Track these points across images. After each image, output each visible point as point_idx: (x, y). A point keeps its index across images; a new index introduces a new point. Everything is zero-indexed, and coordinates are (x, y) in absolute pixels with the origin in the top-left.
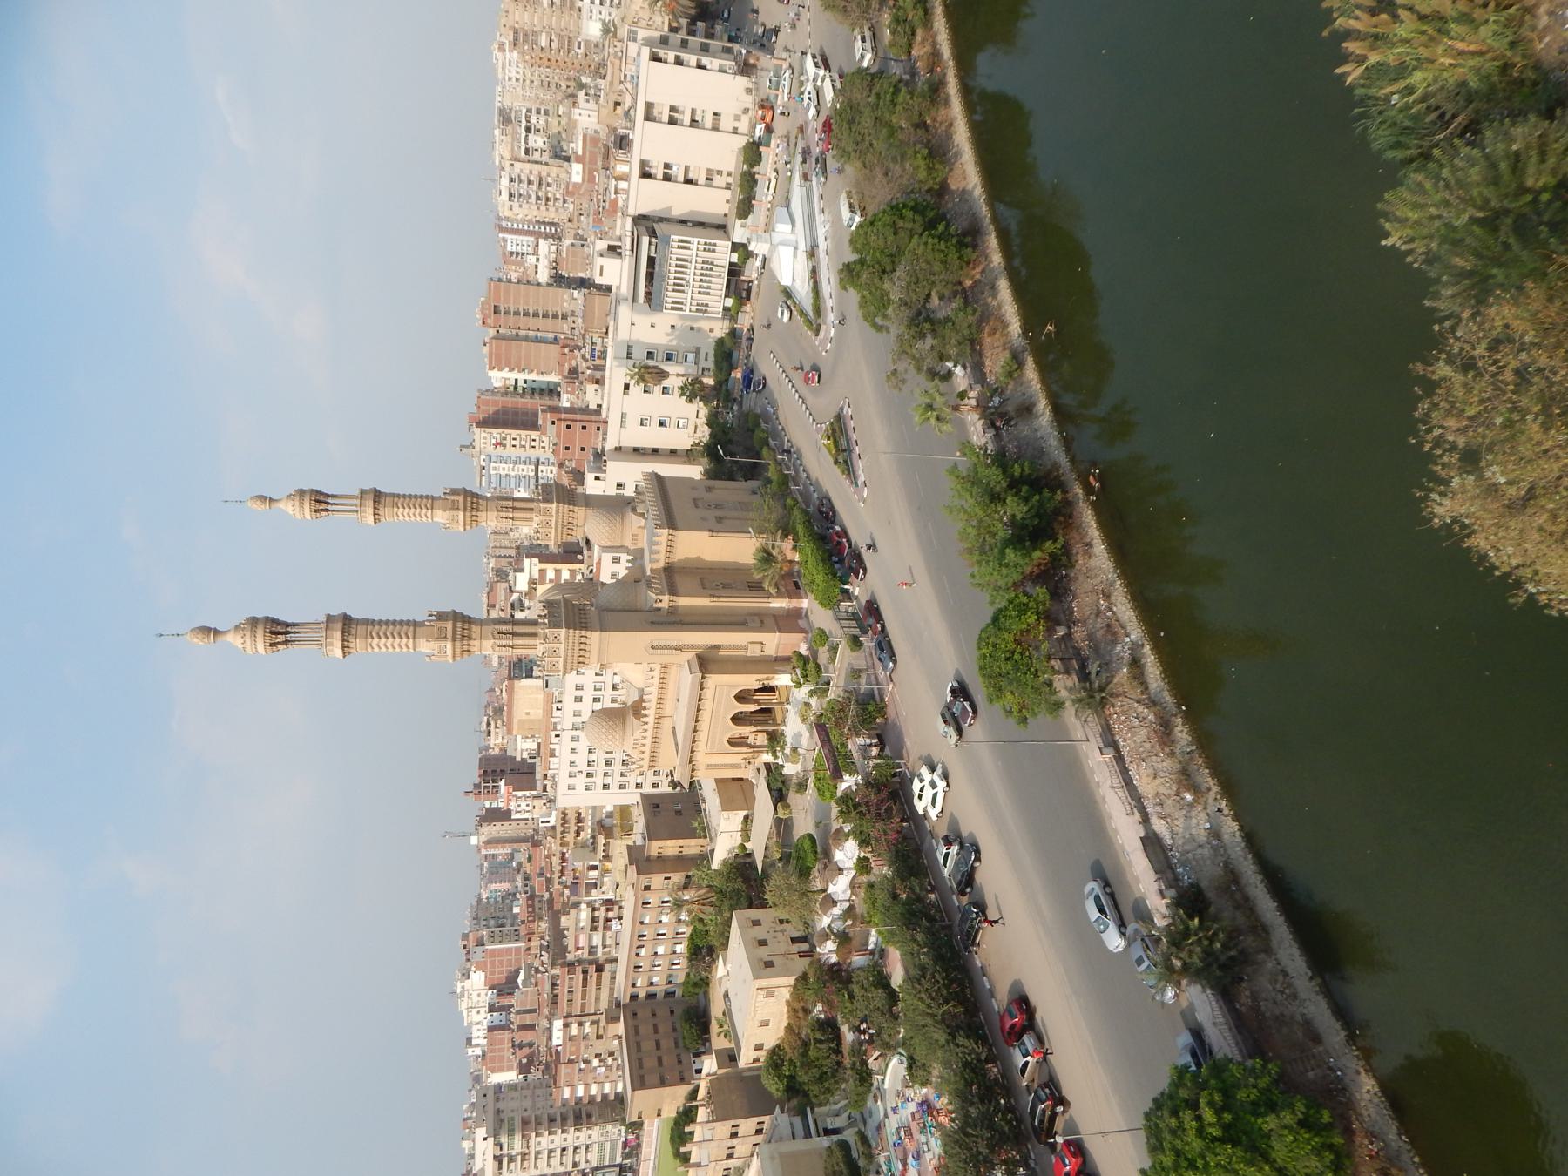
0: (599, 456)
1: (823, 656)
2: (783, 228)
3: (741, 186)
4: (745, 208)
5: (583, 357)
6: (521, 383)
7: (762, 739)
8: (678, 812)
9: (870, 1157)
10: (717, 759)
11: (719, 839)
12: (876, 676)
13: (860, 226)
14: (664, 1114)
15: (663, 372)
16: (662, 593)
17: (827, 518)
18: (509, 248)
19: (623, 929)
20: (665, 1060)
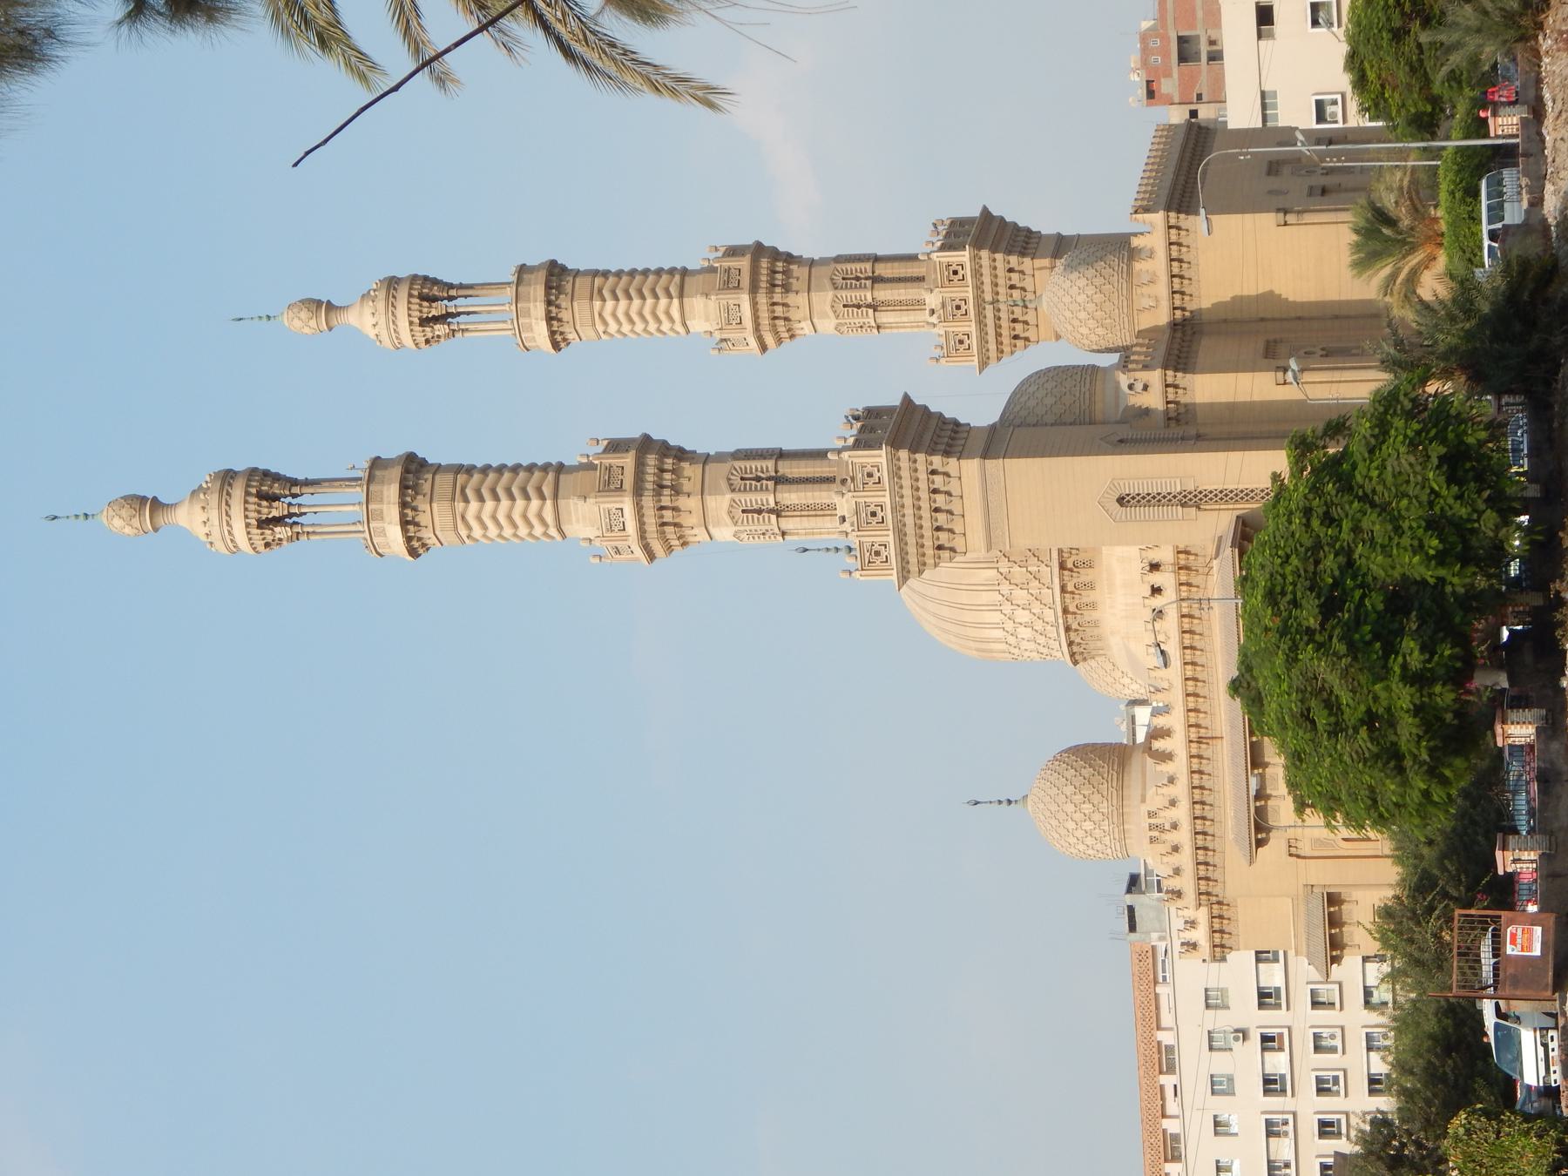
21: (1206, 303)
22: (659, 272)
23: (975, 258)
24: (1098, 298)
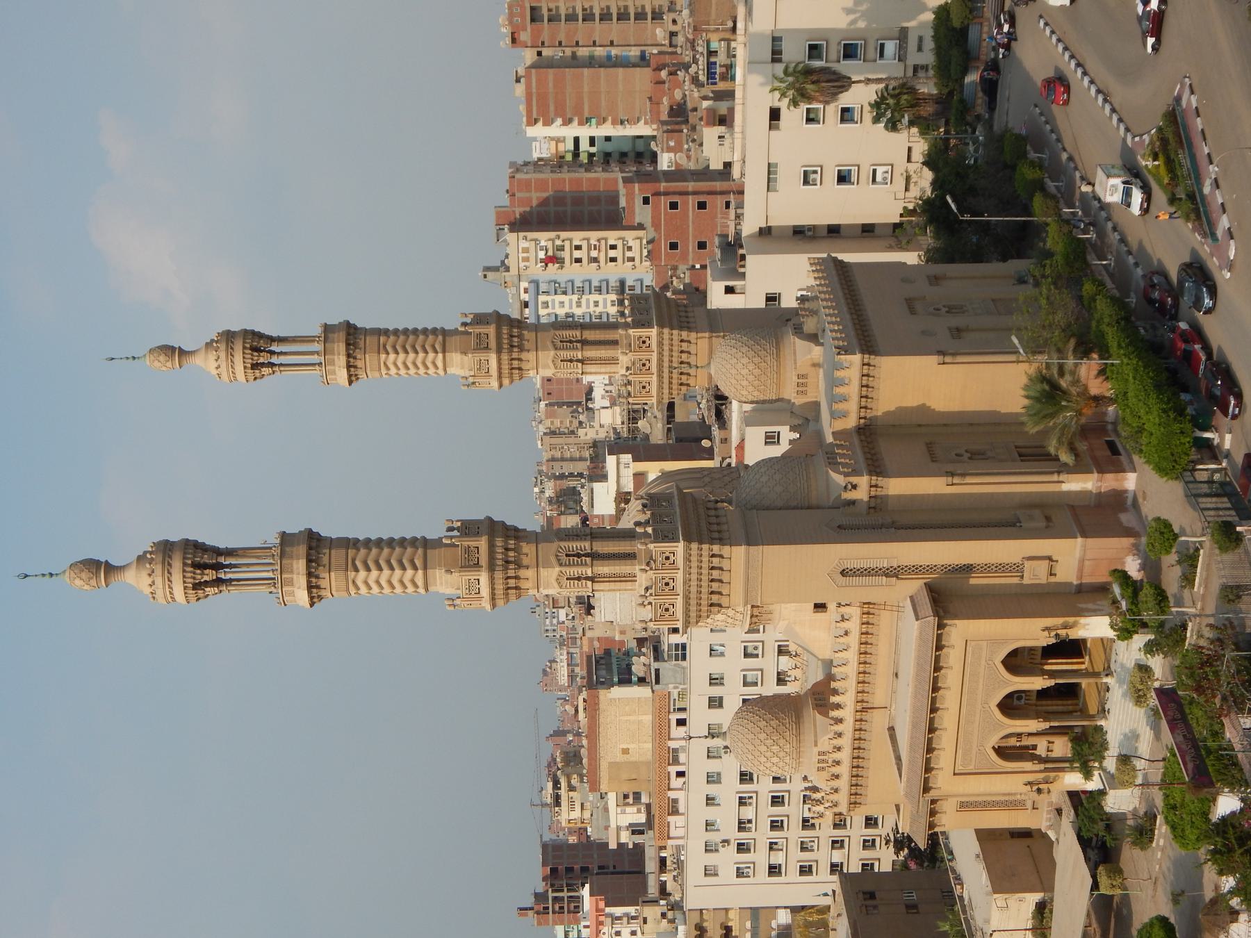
0: (733, 251)
1: (1171, 577)
5: (695, 80)
6: (584, 146)
7: (1061, 746)
8: (911, 907)
10: (980, 792)
16: (856, 472)
21: (880, 414)
22: (425, 331)
23: (660, 334)
24: (757, 372)
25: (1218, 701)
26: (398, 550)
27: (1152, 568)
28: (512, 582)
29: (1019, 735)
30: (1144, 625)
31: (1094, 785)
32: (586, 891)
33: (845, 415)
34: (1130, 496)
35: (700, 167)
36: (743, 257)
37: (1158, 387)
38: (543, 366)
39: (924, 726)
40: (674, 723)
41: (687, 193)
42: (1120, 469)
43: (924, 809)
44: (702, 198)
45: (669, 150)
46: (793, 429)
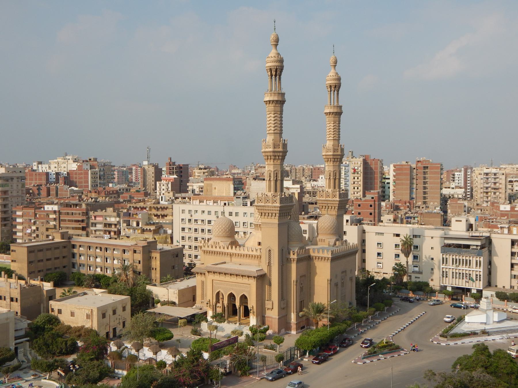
0: (359, 222)
1: (268, 342)
2: (496, 317)
3: (514, 294)
4: (502, 296)
5: (406, 213)
6: (387, 181)
7: (219, 310)
8: (173, 267)
9: (7, 372)
10: (208, 288)
11: (165, 289)
12: (263, 370)
13: (510, 355)
14: (13, 264)
15: (409, 254)
16: (298, 255)
17: (342, 343)
18: (456, 173)
19: (106, 240)
20: (41, 264)
23: (337, 201)
25: (234, 354)
26: (279, 126)
27: (270, 337)
28: (269, 157)
29: (223, 299)
30: (254, 335)
31: (209, 318)
32: (175, 176)
33: (314, 252)
34: (289, 332)
35: (382, 214)
36: (357, 225)
37: (321, 341)
38: (329, 167)
39: (226, 272)
40: (225, 202)
41: (374, 210)
42: (297, 329)
43: (202, 271)
44: (373, 214)
45: (386, 205)
46: (309, 238)
